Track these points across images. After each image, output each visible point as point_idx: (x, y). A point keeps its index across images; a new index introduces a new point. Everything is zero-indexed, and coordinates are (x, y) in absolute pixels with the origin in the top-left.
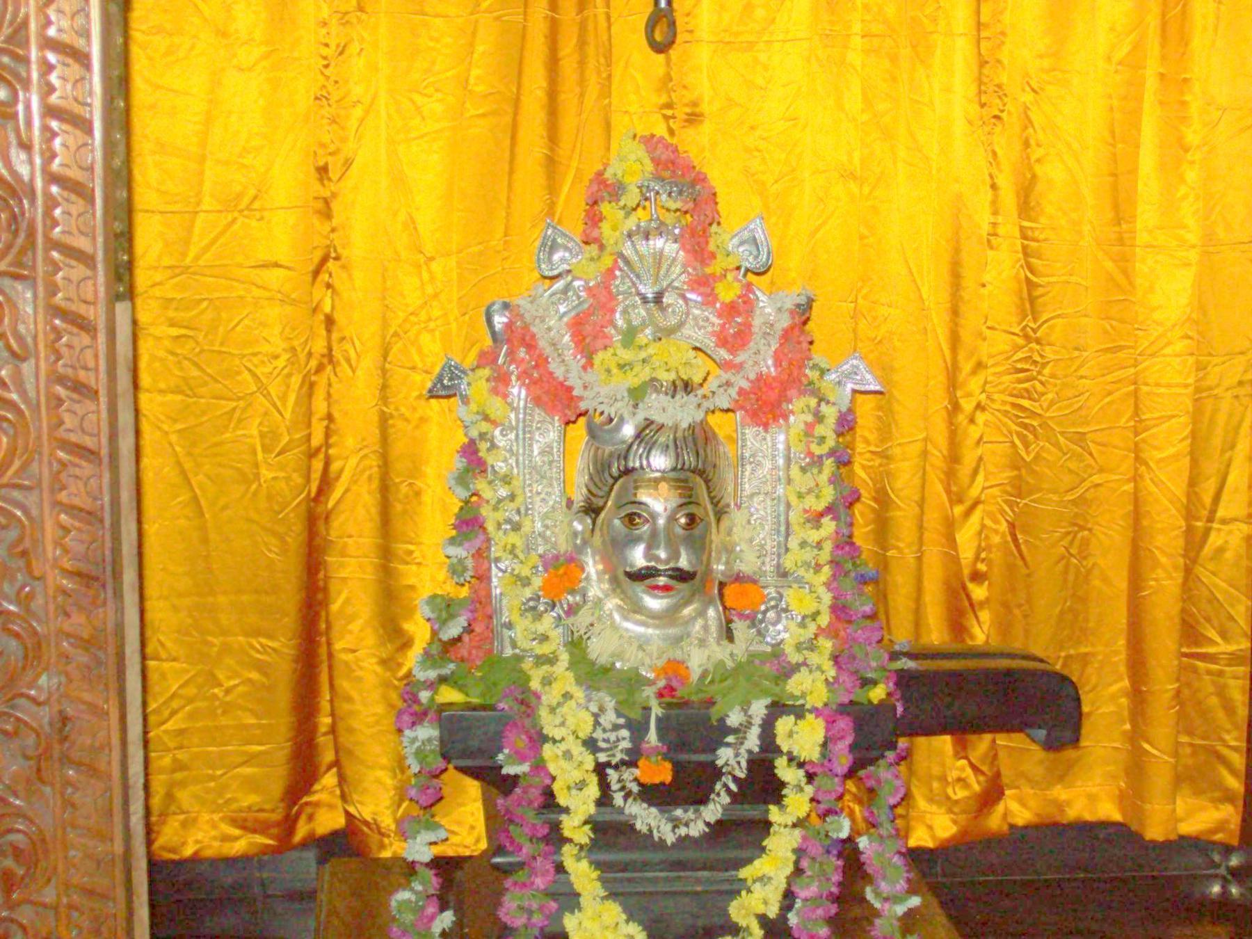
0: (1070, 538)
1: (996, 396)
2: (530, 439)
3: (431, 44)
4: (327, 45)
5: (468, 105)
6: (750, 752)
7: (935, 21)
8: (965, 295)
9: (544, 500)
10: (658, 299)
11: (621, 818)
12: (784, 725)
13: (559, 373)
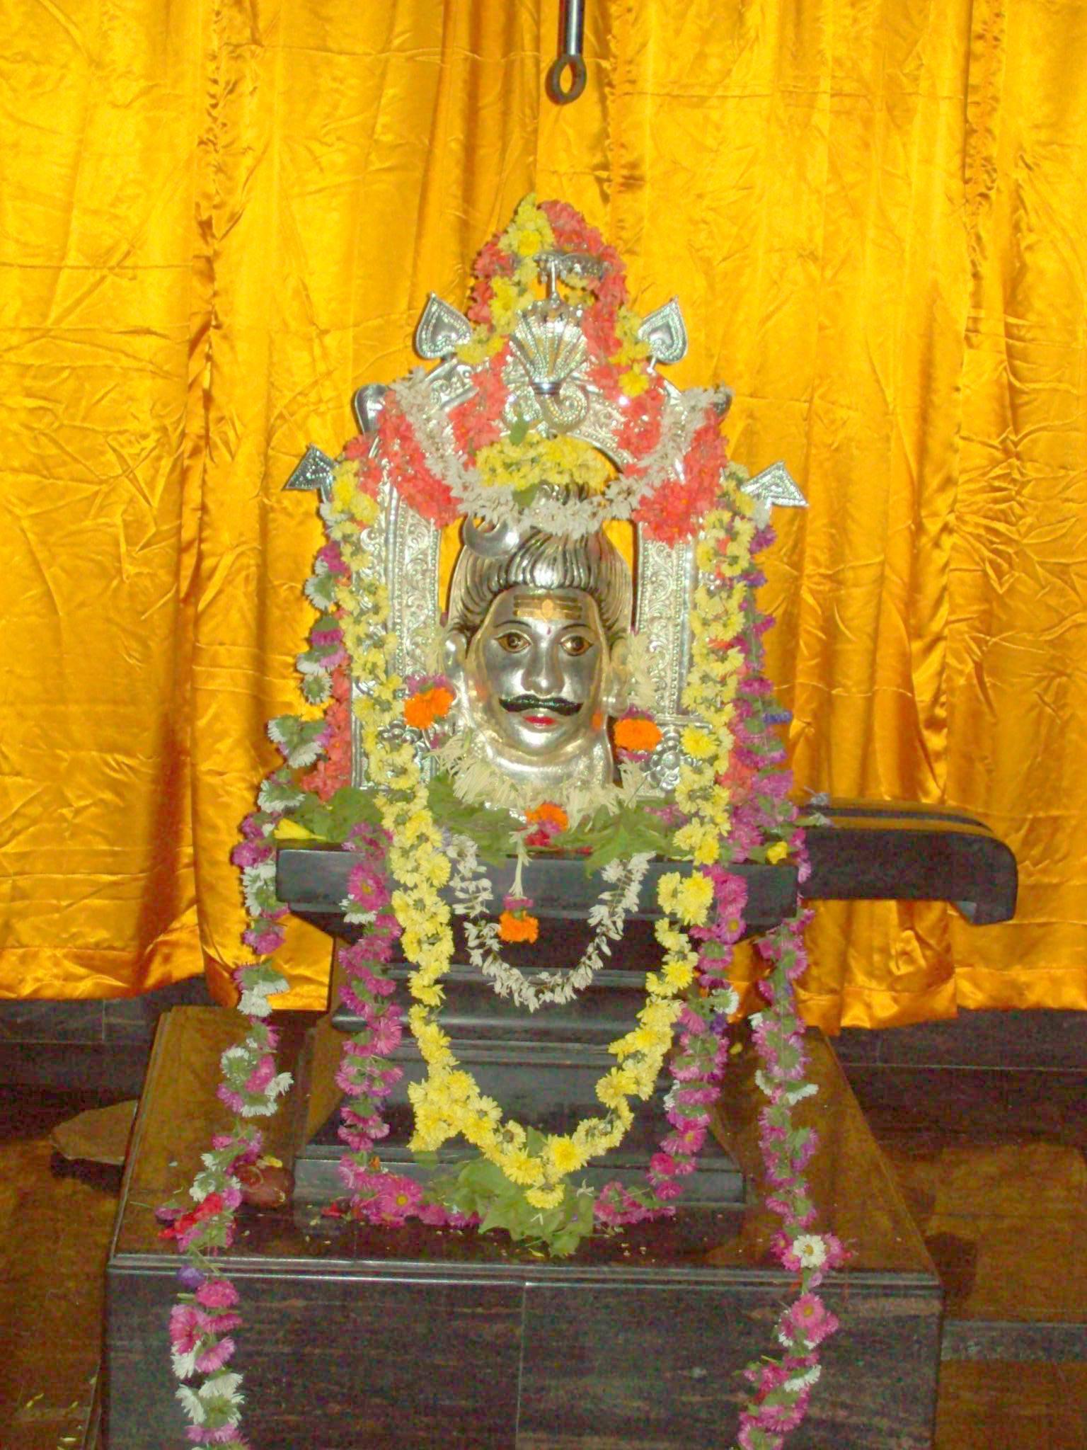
0: (1044, 683)
1: (968, 518)
2: (402, 544)
3: (335, 85)
4: (215, 82)
5: (373, 157)
6: (627, 911)
7: (916, 79)
8: (936, 399)
9: (413, 614)
10: (554, 390)
11: (475, 977)
12: (667, 882)
13: (436, 468)
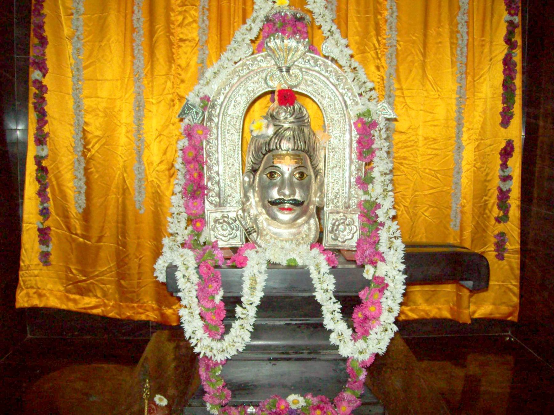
9: (230, 168)
